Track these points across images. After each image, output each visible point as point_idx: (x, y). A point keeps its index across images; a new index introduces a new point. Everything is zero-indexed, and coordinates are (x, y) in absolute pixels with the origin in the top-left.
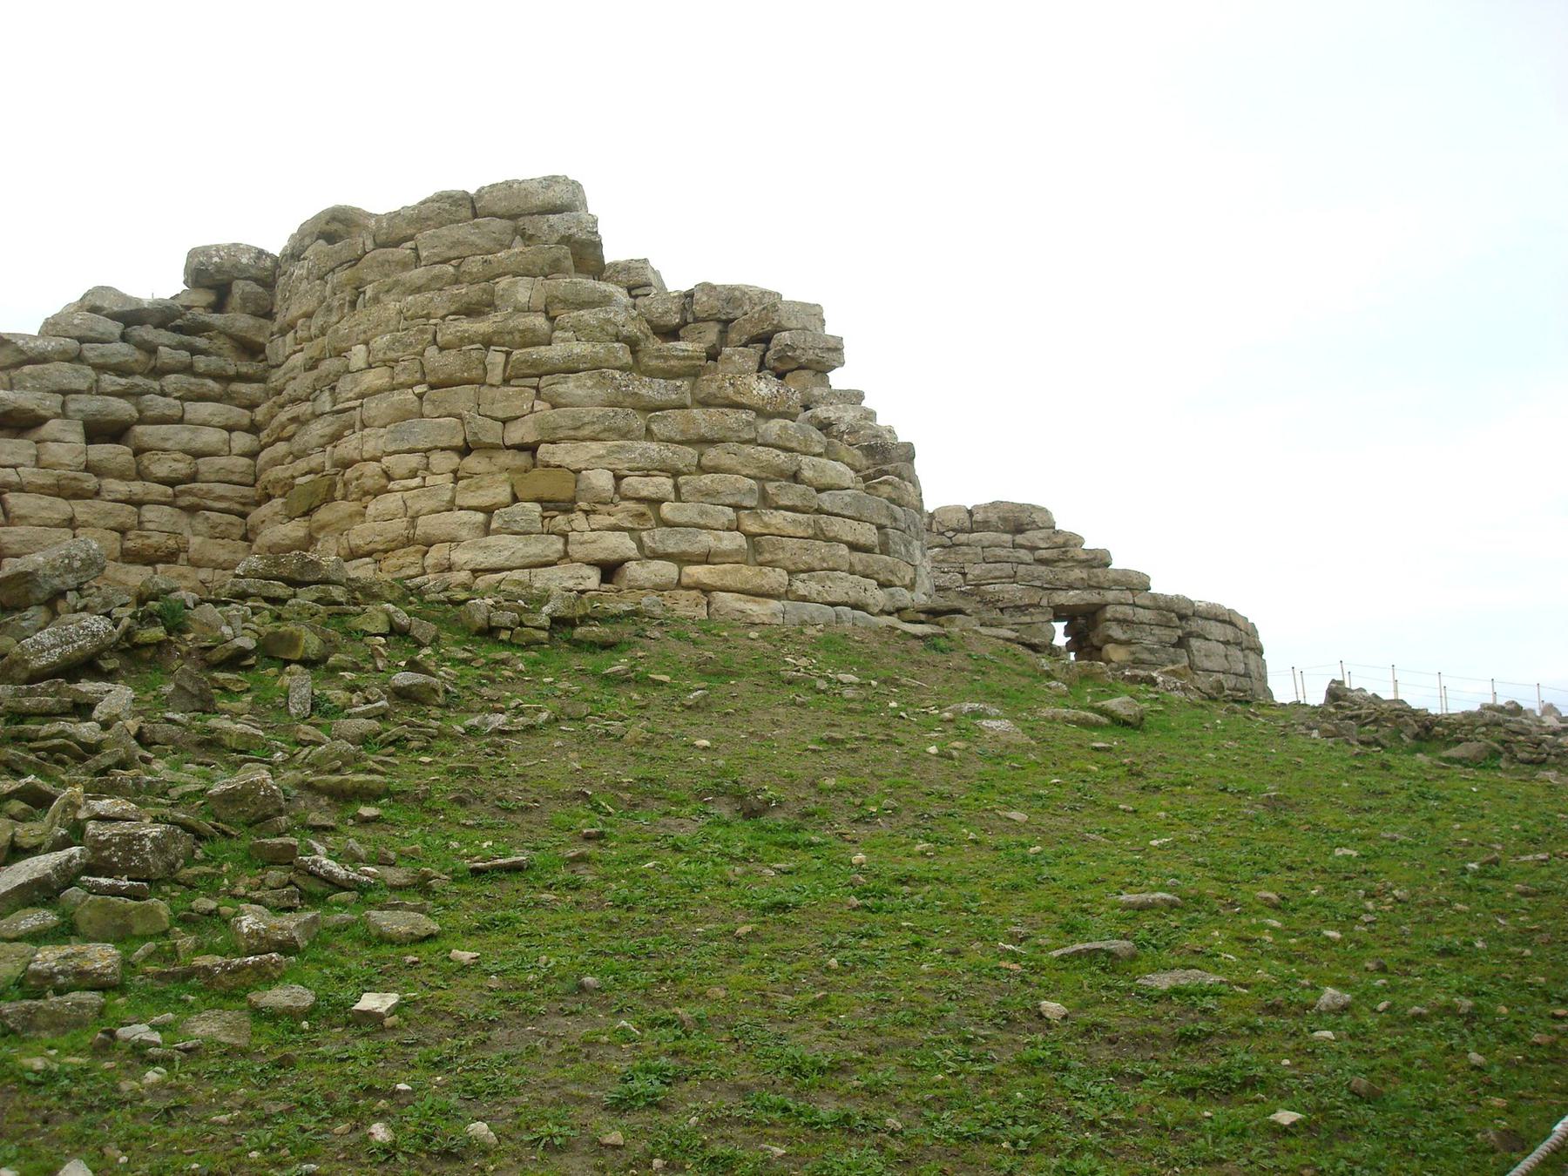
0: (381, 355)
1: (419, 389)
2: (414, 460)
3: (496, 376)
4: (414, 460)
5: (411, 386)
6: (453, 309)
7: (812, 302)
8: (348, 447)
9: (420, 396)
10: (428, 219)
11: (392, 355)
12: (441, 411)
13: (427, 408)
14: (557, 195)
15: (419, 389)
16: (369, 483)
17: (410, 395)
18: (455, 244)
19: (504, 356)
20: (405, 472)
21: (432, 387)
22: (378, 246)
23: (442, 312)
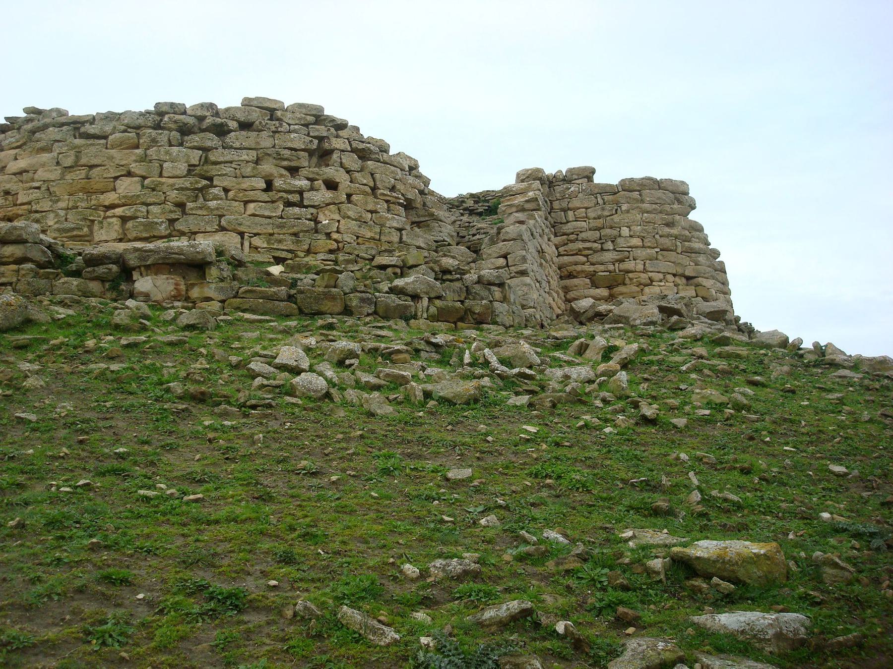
0: (638, 234)
1: (658, 250)
2: (661, 276)
3: (679, 250)
4: (661, 276)
5: (653, 248)
6: (664, 222)
7: (515, 176)
8: (629, 265)
9: (657, 252)
10: (645, 185)
11: (642, 234)
12: (666, 259)
13: (660, 257)
14: (681, 189)
15: (658, 250)
16: (643, 281)
17: (653, 251)
18: (659, 198)
19: (554, 207)
20: (658, 279)
21: (661, 250)
22: (623, 190)
23: (659, 223)
